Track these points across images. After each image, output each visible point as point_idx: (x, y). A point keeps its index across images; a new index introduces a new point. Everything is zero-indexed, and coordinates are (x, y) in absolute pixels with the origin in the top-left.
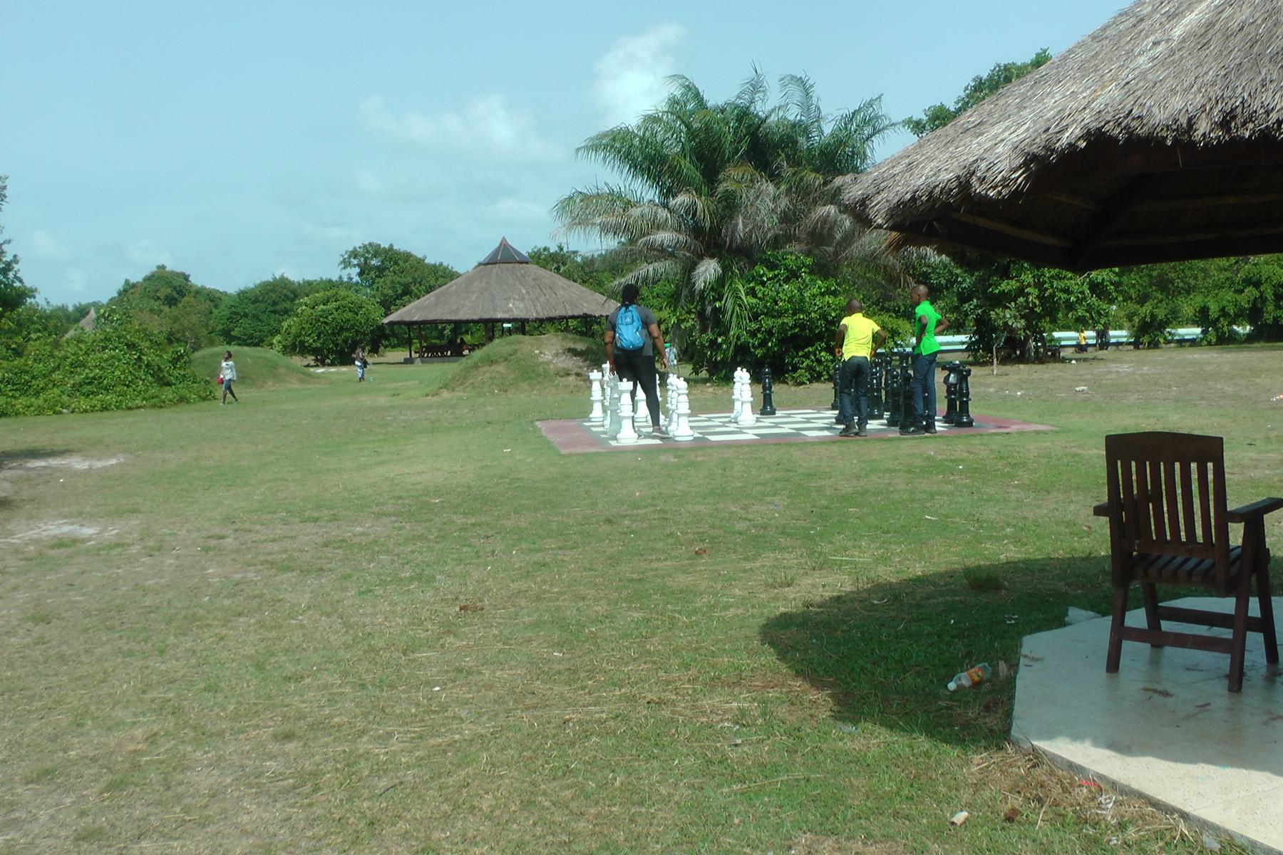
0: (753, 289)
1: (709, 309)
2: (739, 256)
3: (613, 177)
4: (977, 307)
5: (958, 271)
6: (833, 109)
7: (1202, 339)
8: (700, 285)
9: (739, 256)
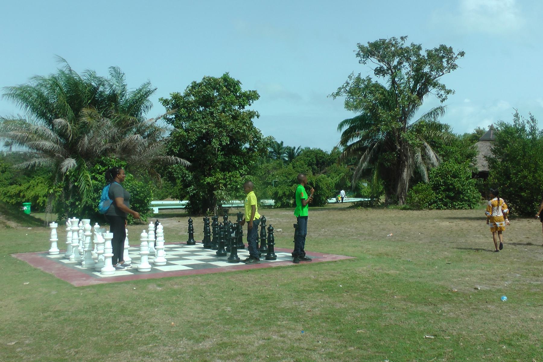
0: (94, 176)
1: (71, 186)
2: (86, 157)
3: (18, 111)
4: (194, 190)
5: (187, 172)
6: (132, 86)
7: (275, 206)
8: (64, 170)
9: (86, 157)
